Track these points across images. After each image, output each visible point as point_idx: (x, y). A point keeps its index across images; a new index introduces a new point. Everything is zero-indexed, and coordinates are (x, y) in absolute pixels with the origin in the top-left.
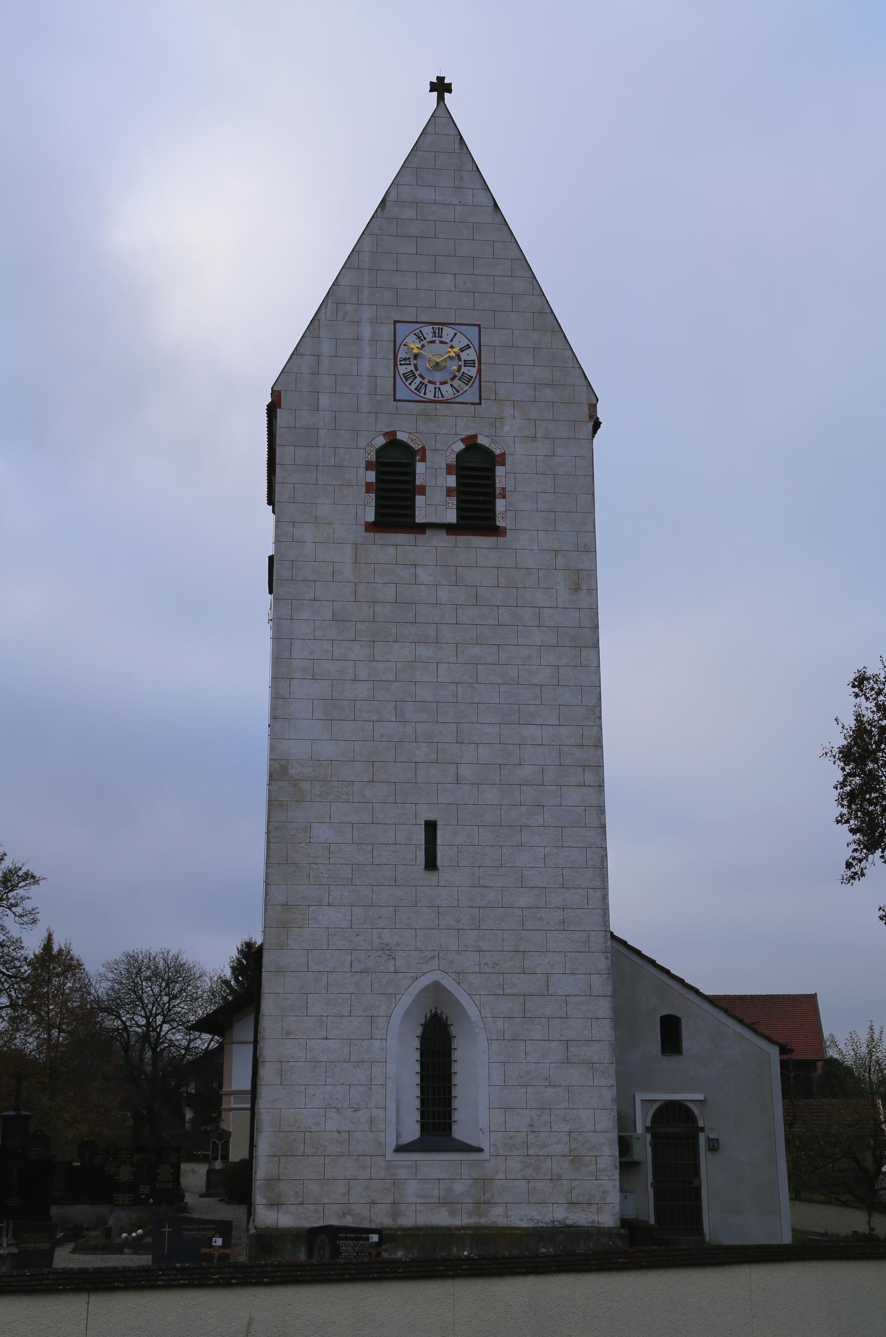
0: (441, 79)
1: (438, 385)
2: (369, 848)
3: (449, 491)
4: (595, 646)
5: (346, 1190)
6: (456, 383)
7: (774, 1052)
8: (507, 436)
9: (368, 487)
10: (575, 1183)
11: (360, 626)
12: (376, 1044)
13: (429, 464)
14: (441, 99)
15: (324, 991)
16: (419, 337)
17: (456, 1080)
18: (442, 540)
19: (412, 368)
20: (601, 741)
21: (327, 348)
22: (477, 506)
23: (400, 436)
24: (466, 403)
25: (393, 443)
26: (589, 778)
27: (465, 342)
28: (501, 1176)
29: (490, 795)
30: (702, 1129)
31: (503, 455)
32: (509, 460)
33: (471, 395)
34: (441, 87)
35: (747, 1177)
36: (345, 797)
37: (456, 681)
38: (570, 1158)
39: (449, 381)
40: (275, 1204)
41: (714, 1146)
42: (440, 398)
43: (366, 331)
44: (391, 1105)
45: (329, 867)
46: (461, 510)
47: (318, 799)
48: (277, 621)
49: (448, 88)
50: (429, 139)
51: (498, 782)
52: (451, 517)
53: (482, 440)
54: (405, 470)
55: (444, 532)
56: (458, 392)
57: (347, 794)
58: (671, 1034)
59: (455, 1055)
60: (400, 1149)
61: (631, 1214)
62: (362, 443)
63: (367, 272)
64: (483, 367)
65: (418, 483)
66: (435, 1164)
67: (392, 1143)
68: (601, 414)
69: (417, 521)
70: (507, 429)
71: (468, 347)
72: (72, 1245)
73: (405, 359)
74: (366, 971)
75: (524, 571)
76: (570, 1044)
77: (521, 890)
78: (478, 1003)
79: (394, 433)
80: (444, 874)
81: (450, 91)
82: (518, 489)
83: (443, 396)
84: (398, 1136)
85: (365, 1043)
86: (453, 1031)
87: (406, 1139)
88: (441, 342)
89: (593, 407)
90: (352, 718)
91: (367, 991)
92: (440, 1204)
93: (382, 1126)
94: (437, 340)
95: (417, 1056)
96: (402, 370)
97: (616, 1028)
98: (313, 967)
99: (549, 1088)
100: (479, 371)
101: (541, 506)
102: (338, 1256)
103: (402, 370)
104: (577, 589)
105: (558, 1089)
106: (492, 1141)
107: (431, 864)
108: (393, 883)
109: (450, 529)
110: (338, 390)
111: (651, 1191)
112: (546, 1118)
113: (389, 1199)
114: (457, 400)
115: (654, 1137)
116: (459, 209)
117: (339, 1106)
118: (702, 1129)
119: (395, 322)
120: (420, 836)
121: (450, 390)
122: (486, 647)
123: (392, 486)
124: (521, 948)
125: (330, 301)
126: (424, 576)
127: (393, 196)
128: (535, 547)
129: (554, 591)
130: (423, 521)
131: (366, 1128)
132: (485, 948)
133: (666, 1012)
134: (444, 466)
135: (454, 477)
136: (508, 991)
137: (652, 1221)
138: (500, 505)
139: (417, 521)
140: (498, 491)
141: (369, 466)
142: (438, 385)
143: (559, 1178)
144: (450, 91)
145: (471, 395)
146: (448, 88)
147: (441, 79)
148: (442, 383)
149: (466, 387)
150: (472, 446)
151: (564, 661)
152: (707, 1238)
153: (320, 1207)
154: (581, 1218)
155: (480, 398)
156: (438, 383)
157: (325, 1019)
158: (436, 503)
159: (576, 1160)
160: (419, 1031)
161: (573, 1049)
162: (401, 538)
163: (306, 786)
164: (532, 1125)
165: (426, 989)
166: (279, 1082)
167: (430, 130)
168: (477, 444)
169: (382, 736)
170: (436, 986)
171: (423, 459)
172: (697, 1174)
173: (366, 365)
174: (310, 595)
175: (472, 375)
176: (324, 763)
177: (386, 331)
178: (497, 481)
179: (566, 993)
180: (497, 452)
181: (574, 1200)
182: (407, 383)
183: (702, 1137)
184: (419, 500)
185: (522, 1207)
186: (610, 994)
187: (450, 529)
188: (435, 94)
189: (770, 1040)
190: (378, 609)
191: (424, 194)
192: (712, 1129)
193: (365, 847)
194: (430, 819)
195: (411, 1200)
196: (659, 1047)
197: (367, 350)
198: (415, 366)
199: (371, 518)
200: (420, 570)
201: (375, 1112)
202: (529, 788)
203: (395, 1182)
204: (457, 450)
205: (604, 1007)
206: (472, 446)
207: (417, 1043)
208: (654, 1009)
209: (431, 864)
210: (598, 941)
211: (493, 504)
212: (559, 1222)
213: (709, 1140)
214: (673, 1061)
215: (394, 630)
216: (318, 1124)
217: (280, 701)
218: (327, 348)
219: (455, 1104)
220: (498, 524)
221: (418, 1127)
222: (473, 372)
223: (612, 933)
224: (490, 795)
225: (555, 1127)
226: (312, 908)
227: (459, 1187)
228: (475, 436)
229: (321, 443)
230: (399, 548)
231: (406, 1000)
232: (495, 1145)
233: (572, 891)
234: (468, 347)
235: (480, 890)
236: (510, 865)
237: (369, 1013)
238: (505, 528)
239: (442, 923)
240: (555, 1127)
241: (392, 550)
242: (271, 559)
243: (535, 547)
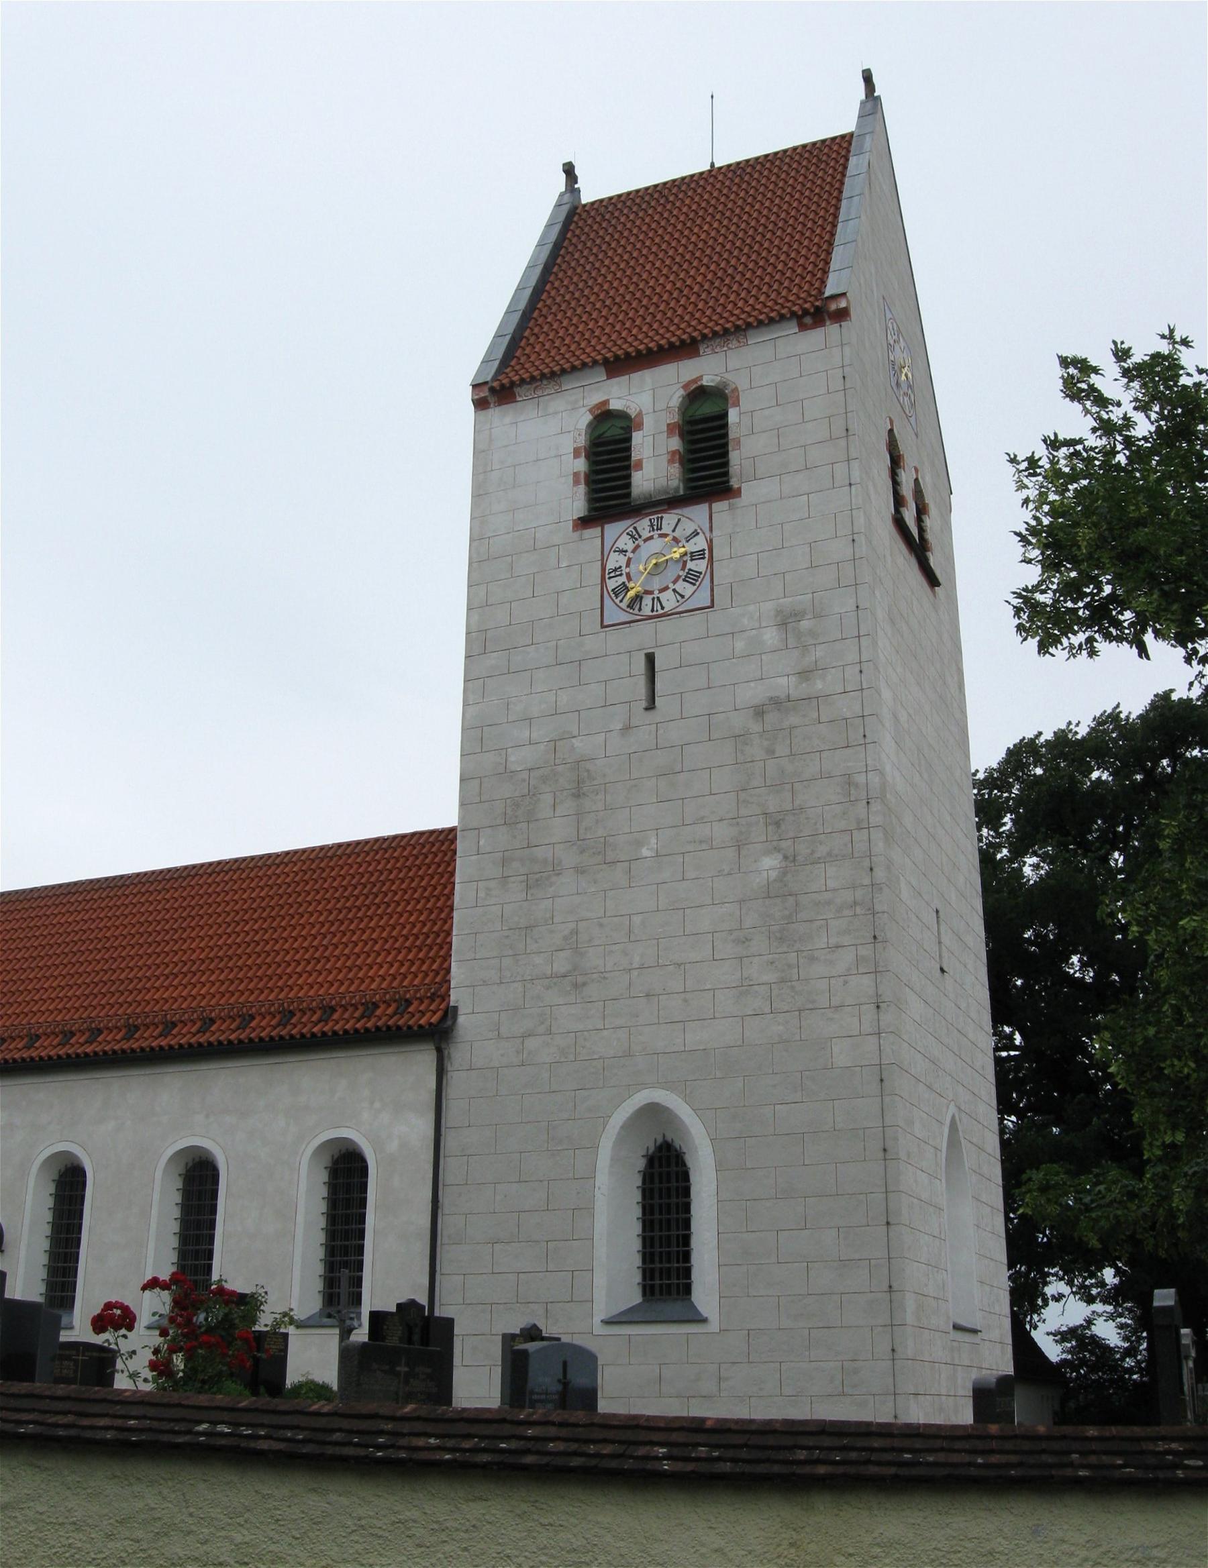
1: (629, 554)
19: (624, 579)
39: (671, 585)
42: (661, 612)
56: (683, 597)
73: (615, 570)
83: (663, 608)
96: (612, 584)
120: (640, 665)
142: (656, 594)
148: (661, 591)
155: (712, 601)
156: (656, 592)
222: (701, 566)
228: (606, 402)
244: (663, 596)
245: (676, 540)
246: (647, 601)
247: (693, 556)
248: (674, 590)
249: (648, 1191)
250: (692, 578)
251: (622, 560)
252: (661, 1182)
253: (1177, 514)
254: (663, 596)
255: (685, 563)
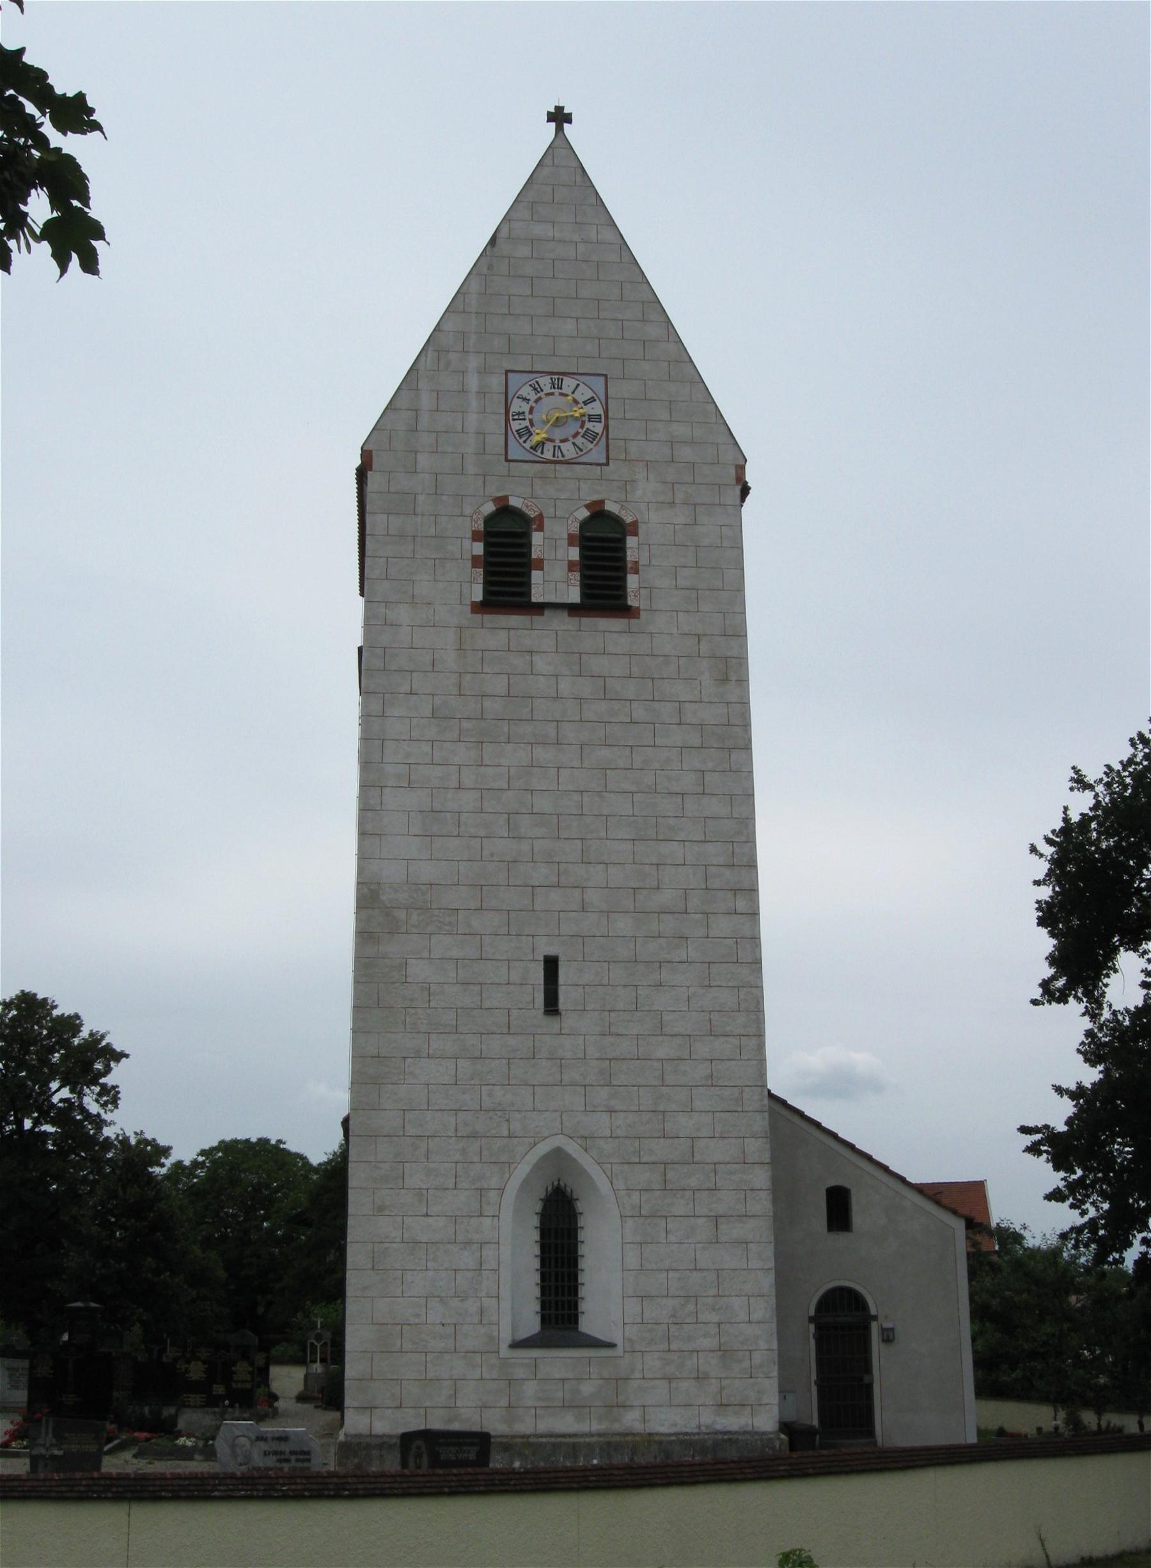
0: (559, 109)
2: (478, 988)
3: (571, 566)
4: (747, 747)
5: (452, 1392)
6: (579, 440)
7: (959, 1226)
8: (639, 501)
9: (475, 561)
10: (724, 1383)
11: (466, 725)
12: (487, 1221)
13: (547, 533)
14: (559, 129)
15: (423, 1159)
16: (535, 389)
17: (582, 1264)
18: (562, 623)
20: (755, 861)
21: (426, 401)
22: (605, 577)
23: (514, 502)
24: (591, 464)
25: (504, 510)
26: (742, 904)
27: (589, 394)
28: (638, 1375)
29: (623, 924)
30: (875, 1318)
31: (635, 524)
32: (642, 529)
33: (596, 454)
34: (559, 117)
35: (926, 1371)
36: (447, 928)
37: (582, 789)
38: (720, 1353)
40: (368, 1409)
41: (888, 1337)
42: (561, 458)
43: (473, 382)
44: (505, 1292)
45: (428, 1011)
46: (585, 587)
47: (415, 930)
48: (366, 718)
49: (568, 119)
50: (546, 171)
51: (632, 909)
52: (574, 595)
53: (610, 507)
54: (518, 541)
55: (565, 613)
56: (581, 450)
57: (450, 924)
58: (839, 1209)
59: (582, 1235)
60: (516, 1345)
61: (791, 1416)
62: (468, 510)
63: (474, 316)
64: (611, 422)
65: (534, 556)
66: (558, 1362)
67: (506, 1336)
68: (749, 478)
69: (534, 600)
70: (639, 493)
71: (592, 400)
72: (134, 1451)
73: (519, 414)
74: (474, 1136)
75: (661, 659)
76: (720, 1220)
77: (660, 1038)
78: (609, 1174)
79: (506, 498)
80: (569, 1020)
81: (570, 122)
82: (653, 562)
83: (563, 456)
84: (514, 1329)
85: (473, 1220)
86: (580, 1206)
87: (523, 1334)
88: (561, 394)
89: (741, 469)
90: (456, 833)
91: (476, 1159)
92: (566, 1406)
93: (494, 1319)
94: (556, 391)
95: (536, 1235)
96: (515, 425)
97: (775, 1201)
98: (411, 1130)
99: (695, 1273)
100: (606, 427)
101: (681, 582)
102: (449, 1464)
103: (515, 425)
104: (725, 680)
105: (705, 1273)
106: (627, 1334)
107: (552, 1005)
108: (505, 1030)
109: (572, 609)
110: (440, 449)
111: (814, 1389)
112: (691, 1307)
113: (504, 1402)
114: (580, 460)
115: (819, 1328)
116: (581, 247)
117: (443, 1294)
118: (875, 1318)
119: (507, 372)
120: (538, 974)
121: (572, 448)
122: (616, 748)
123: (506, 579)
124: (661, 1108)
125: (431, 349)
126: (541, 664)
127: (504, 233)
128: (674, 631)
129: (697, 682)
130: (541, 600)
131: (476, 1319)
132: (616, 1108)
133: (832, 1182)
134: (566, 536)
135: (578, 549)
136: (644, 1159)
137: (815, 1423)
138: (632, 581)
139: (534, 600)
140: (629, 565)
141: (475, 537)
143: (706, 1377)
144: (570, 122)
145: (597, 455)
146: (568, 119)
147: (559, 109)
148: (563, 441)
149: (592, 446)
150: (598, 514)
151: (710, 765)
152: (879, 1443)
153: (422, 1411)
154: (732, 1422)
156: (557, 441)
157: (425, 1192)
158: (556, 577)
159: (725, 1353)
160: (539, 1207)
161: (722, 1227)
162: (515, 620)
163: (401, 915)
164: (674, 1316)
165: (546, 1158)
166: (370, 1266)
167: (548, 161)
168: (604, 511)
169: (492, 855)
170: (558, 1154)
171: (541, 528)
172: (868, 1369)
173: (472, 420)
174: (407, 688)
175: (597, 429)
176: (423, 887)
177: (496, 382)
178: (628, 553)
179: (716, 1160)
180: (629, 520)
181: (724, 1402)
182: (521, 441)
183: (874, 1327)
184: (536, 576)
185: (666, 1412)
186: (768, 1161)
187: (572, 609)
188: (553, 124)
189: (955, 1212)
190: (487, 703)
191: (539, 230)
192: (886, 1317)
193: (472, 987)
194: (550, 953)
195: (530, 1403)
196: (825, 1223)
197: (474, 404)
198: (531, 421)
199: (478, 596)
200: (536, 658)
201: (487, 1302)
202: (669, 917)
203: (510, 1381)
204: (581, 518)
205: (761, 1178)
206: (598, 514)
207: (535, 1221)
208: (824, 1182)
209: (552, 1005)
210: (754, 1100)
211: (623, 579)
212: (707, 1427)
213: (883, 1330)
214: (841, 1239)
215: (506, 729)
216: (417, 1315)
217: (369, 814)
218: (426, 401)
219: (582, 1292)
220: (630, 603)
221: (537, 1320)
222: (598, 428)
223: (769, 1091)
224: (623, 924)
225: (702, 1318)
226: (408, 1061)
227: (587, 1388)
228: (602, 502)
229: (419, 510)
230: (512, 632)
231: (523, 1170)
232: (630, 1340)
233: (722, 1039)
234: (592, 400)
235: (611, 1039)
236: (647, 1008)
237: (478, 1185)
238: (638, 609)
239: (566, 1078)
240: (702, 1318)
241: (503, 635)
242: (360, 649)
243: (674, 631)
244: (564, 446)
245: (576, 402)
246: (549, 446)
247: (591, 418)
248: (574, 444)
249: (546, 1232)
250: (592, 437)
251: (525, 408)
252: (557, 1281)
253: (1105, 1036)
254: (564, 446)
255: (583, 423)
